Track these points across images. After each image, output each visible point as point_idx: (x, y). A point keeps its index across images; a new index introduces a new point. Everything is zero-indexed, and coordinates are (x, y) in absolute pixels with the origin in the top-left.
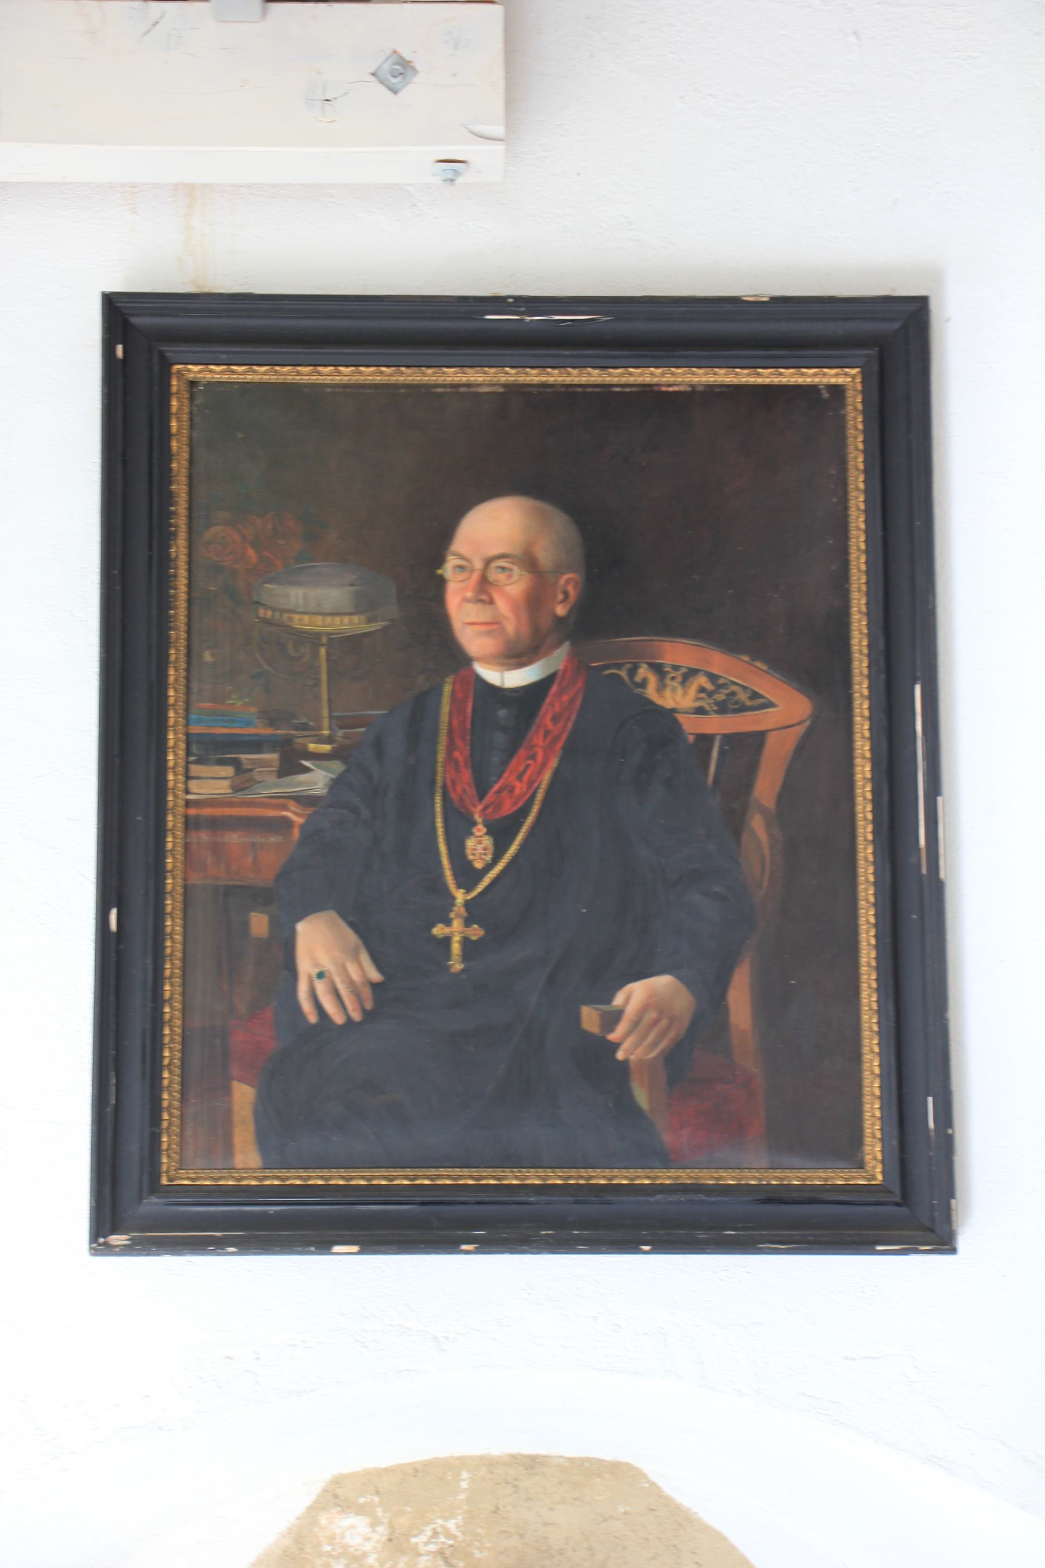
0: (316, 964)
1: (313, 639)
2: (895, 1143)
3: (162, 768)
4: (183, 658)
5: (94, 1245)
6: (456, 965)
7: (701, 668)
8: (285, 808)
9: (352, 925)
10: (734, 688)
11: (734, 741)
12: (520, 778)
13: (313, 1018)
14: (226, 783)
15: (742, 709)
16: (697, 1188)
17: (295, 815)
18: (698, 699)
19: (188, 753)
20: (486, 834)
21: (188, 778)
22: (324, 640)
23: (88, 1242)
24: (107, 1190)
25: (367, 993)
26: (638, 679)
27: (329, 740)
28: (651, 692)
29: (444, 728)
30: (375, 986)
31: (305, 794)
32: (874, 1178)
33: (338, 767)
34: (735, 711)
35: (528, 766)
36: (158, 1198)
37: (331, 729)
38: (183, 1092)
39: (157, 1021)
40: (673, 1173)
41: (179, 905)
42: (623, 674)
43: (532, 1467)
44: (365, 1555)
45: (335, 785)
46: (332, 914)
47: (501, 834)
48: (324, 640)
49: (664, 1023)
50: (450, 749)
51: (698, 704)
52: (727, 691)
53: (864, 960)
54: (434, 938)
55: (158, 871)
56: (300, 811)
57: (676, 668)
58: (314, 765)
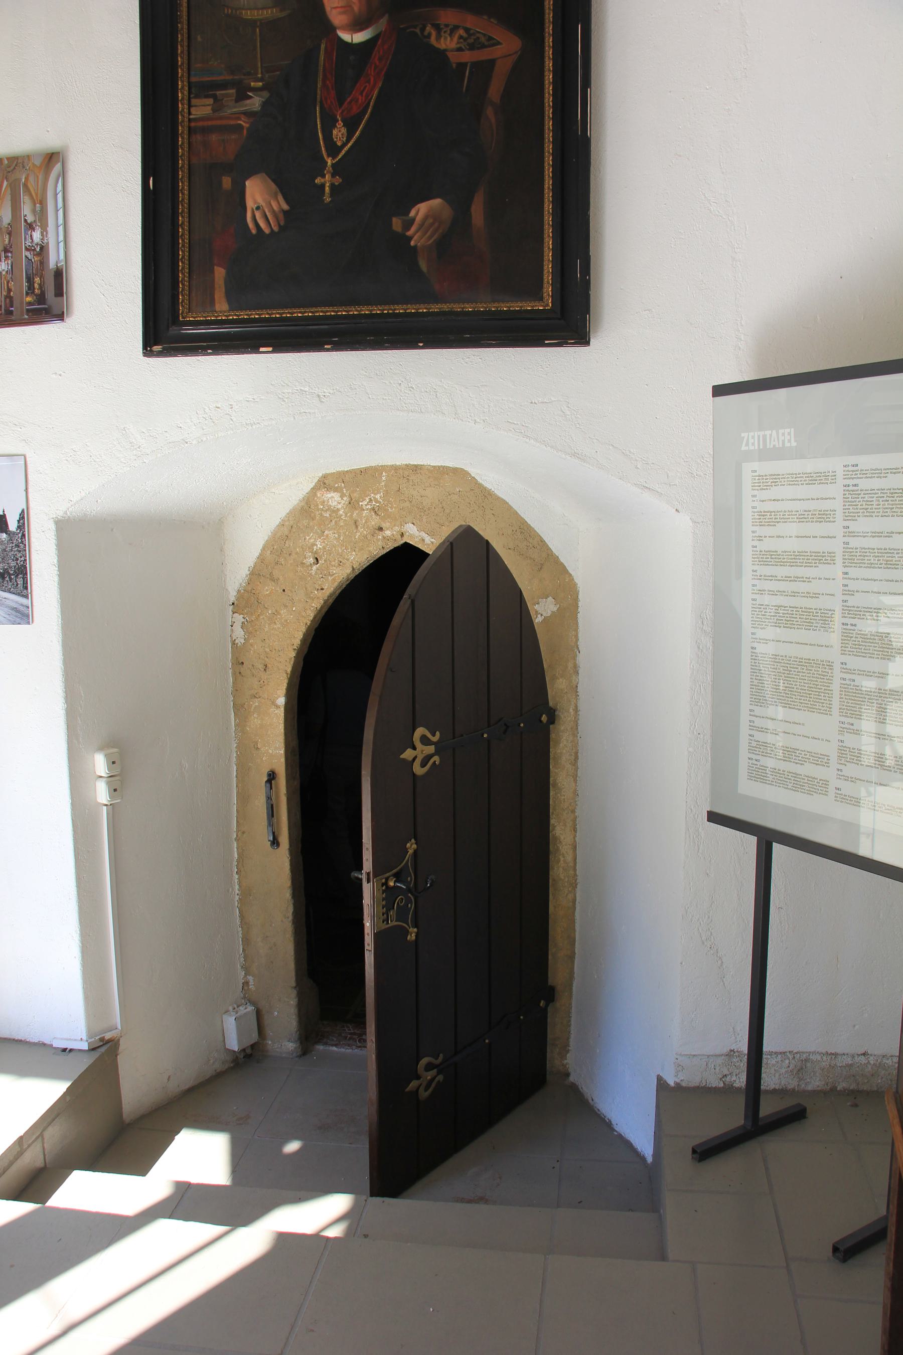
0: (255, 202)
1: (253, 23)
2: (558, 285)
3: (175, 101)
4: (186, 40)
5: (145, 351)
6: (327, 199)
7: (495, 37)
8: (239, 119)
9: (274, 181)
10: (478, 35)
11: (476, 65)
12: (361, 94)
13: (254, 232)
14: (210, 108)
15: (483, 46)
16: (452, 313)
17: (244, 123)
18: (458, 43)
19: (190, 93)
20: (342, 126)
21: (190, 106)
22: (258, 24)
23: (142, 350)
24: (151, 324)
25: (281, 216)
26: (426, 33)
27: (261, 80)
28: (433, 40)
29: (321, 68)
30: (285, 213)
31: (249, 111)
32: (548, 305)
33: (266, 94)
34: (478, 49)
35: (366, 86)
36: (176, 327)
37: (262, 73)
38: (189, 273)
39: (175, 236)
40: (439, 306)
41: (186, 175)
42: (418, 31)
43: (416, 470)
44: (338, 510)
45: (264, 105)
46: (264, 174)
47: (351, 127)
48: (258, 24)
49: (437, 224)
50: (324, 81)
51: (458, 46)
52: (475, 37)
53: (546, 186)
54: (316, 185)
55: (174, 157)
56: (247, 121)
57: (447, 26)
58: (253, 94)
